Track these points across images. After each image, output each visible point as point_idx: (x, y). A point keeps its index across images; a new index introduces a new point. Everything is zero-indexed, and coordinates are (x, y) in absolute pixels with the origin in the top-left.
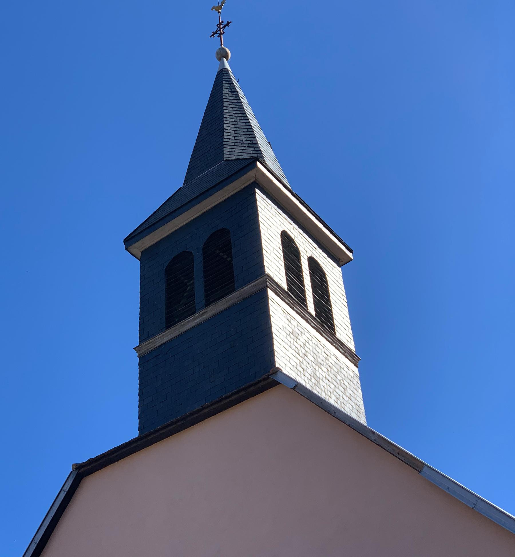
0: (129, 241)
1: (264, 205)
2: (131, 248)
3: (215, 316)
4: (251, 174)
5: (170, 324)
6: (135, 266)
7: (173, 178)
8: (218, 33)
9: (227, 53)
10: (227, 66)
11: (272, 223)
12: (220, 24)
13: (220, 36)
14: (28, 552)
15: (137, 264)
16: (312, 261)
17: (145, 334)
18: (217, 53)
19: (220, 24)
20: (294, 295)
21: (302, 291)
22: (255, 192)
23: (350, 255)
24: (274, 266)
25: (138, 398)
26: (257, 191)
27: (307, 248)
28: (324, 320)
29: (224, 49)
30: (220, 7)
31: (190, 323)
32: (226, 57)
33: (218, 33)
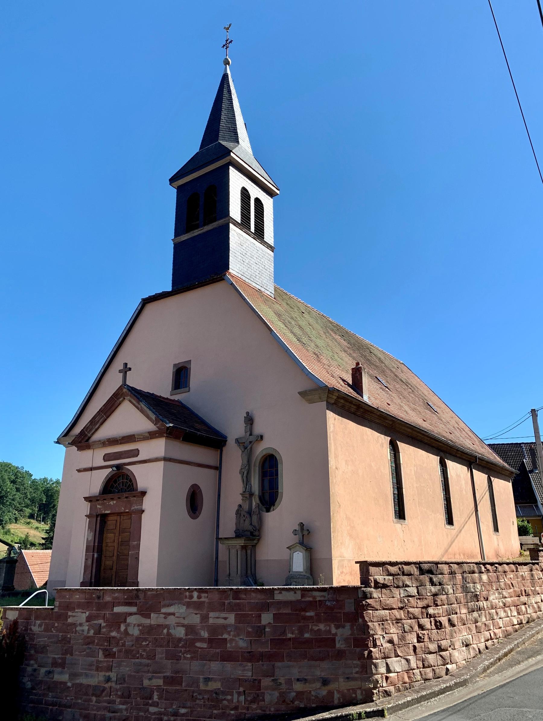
0: (172, 180)
1: (233, 173)
2: (173, 184)
3: (207, 232)
4: (228, 158)
5: (187, 231)
6: (174, 192)
7: (195, 148)
8: (226, 46)
9: (229, 62)
10: (229, 72)
11: (236, 182)
12: (227, 40)
13: (226, 49)
14: (245, 558)
15: (175, 190)
16: (257, 201)
17: (177, 234)
18: (224, 62)
19: (227, 40)
20: (244, 224)
21: (249, 219)
22: (229, 169)
23: (278, 192)
24: (235, 210)
25: (173, 257)
26: (230, 167)
27: (255, 192)
28: (259, 234)
29: (227, 59)
30: (228, 29)
31: (196, 233)
32: (228, 64)
33: (226, 46)
